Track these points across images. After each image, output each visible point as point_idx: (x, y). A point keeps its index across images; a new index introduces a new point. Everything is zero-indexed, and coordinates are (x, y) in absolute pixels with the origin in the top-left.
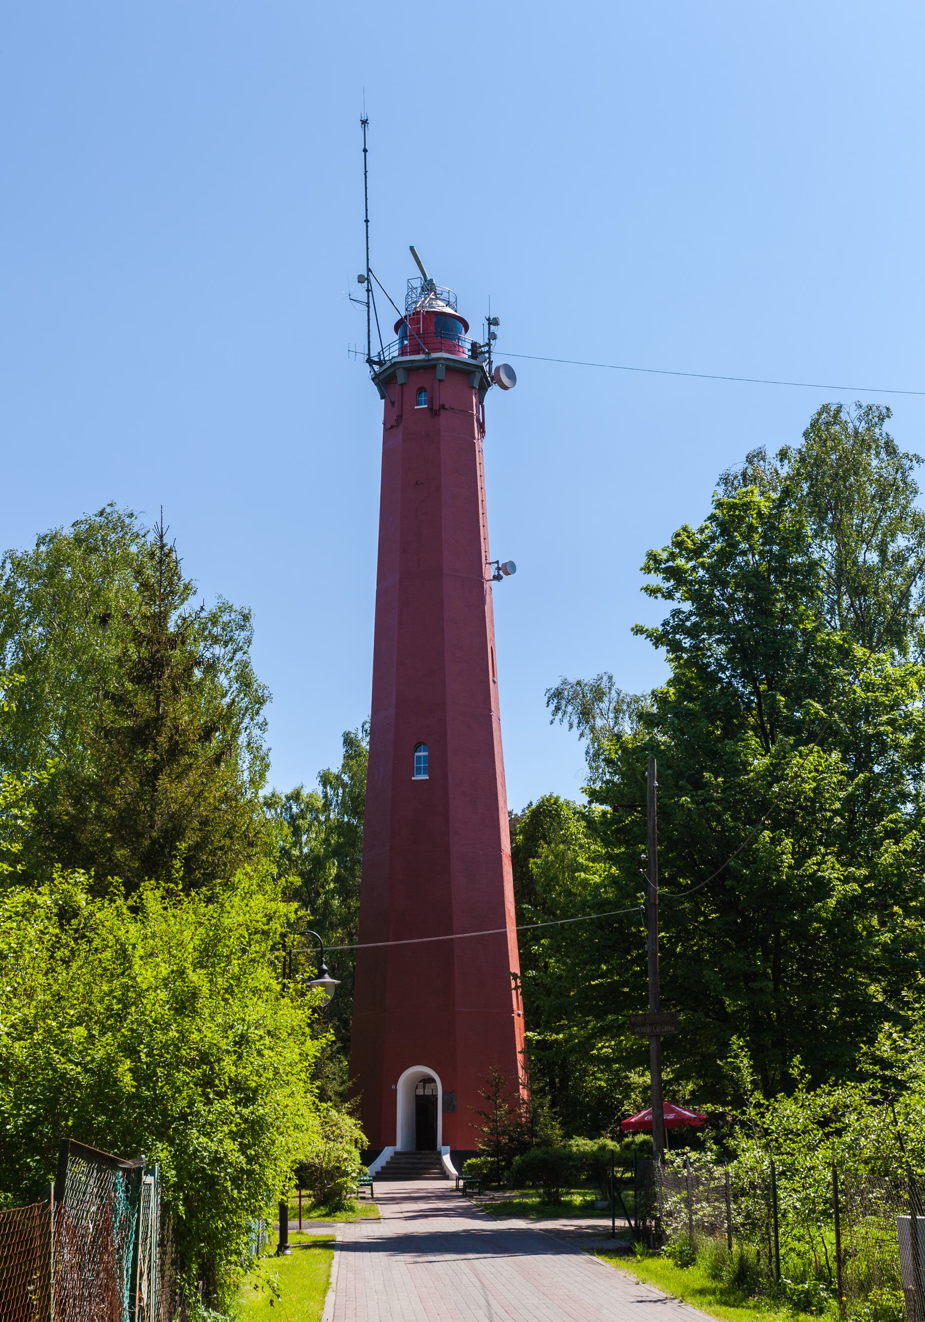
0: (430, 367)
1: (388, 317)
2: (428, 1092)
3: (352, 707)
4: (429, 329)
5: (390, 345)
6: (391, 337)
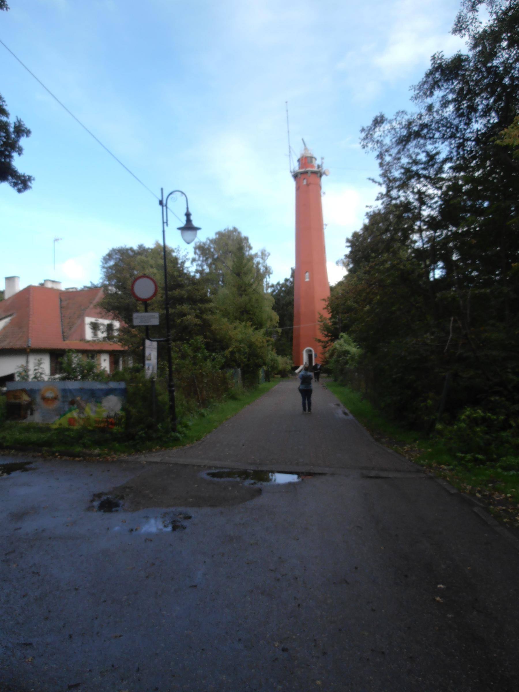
0: (306, 173)
5: (296, 166)
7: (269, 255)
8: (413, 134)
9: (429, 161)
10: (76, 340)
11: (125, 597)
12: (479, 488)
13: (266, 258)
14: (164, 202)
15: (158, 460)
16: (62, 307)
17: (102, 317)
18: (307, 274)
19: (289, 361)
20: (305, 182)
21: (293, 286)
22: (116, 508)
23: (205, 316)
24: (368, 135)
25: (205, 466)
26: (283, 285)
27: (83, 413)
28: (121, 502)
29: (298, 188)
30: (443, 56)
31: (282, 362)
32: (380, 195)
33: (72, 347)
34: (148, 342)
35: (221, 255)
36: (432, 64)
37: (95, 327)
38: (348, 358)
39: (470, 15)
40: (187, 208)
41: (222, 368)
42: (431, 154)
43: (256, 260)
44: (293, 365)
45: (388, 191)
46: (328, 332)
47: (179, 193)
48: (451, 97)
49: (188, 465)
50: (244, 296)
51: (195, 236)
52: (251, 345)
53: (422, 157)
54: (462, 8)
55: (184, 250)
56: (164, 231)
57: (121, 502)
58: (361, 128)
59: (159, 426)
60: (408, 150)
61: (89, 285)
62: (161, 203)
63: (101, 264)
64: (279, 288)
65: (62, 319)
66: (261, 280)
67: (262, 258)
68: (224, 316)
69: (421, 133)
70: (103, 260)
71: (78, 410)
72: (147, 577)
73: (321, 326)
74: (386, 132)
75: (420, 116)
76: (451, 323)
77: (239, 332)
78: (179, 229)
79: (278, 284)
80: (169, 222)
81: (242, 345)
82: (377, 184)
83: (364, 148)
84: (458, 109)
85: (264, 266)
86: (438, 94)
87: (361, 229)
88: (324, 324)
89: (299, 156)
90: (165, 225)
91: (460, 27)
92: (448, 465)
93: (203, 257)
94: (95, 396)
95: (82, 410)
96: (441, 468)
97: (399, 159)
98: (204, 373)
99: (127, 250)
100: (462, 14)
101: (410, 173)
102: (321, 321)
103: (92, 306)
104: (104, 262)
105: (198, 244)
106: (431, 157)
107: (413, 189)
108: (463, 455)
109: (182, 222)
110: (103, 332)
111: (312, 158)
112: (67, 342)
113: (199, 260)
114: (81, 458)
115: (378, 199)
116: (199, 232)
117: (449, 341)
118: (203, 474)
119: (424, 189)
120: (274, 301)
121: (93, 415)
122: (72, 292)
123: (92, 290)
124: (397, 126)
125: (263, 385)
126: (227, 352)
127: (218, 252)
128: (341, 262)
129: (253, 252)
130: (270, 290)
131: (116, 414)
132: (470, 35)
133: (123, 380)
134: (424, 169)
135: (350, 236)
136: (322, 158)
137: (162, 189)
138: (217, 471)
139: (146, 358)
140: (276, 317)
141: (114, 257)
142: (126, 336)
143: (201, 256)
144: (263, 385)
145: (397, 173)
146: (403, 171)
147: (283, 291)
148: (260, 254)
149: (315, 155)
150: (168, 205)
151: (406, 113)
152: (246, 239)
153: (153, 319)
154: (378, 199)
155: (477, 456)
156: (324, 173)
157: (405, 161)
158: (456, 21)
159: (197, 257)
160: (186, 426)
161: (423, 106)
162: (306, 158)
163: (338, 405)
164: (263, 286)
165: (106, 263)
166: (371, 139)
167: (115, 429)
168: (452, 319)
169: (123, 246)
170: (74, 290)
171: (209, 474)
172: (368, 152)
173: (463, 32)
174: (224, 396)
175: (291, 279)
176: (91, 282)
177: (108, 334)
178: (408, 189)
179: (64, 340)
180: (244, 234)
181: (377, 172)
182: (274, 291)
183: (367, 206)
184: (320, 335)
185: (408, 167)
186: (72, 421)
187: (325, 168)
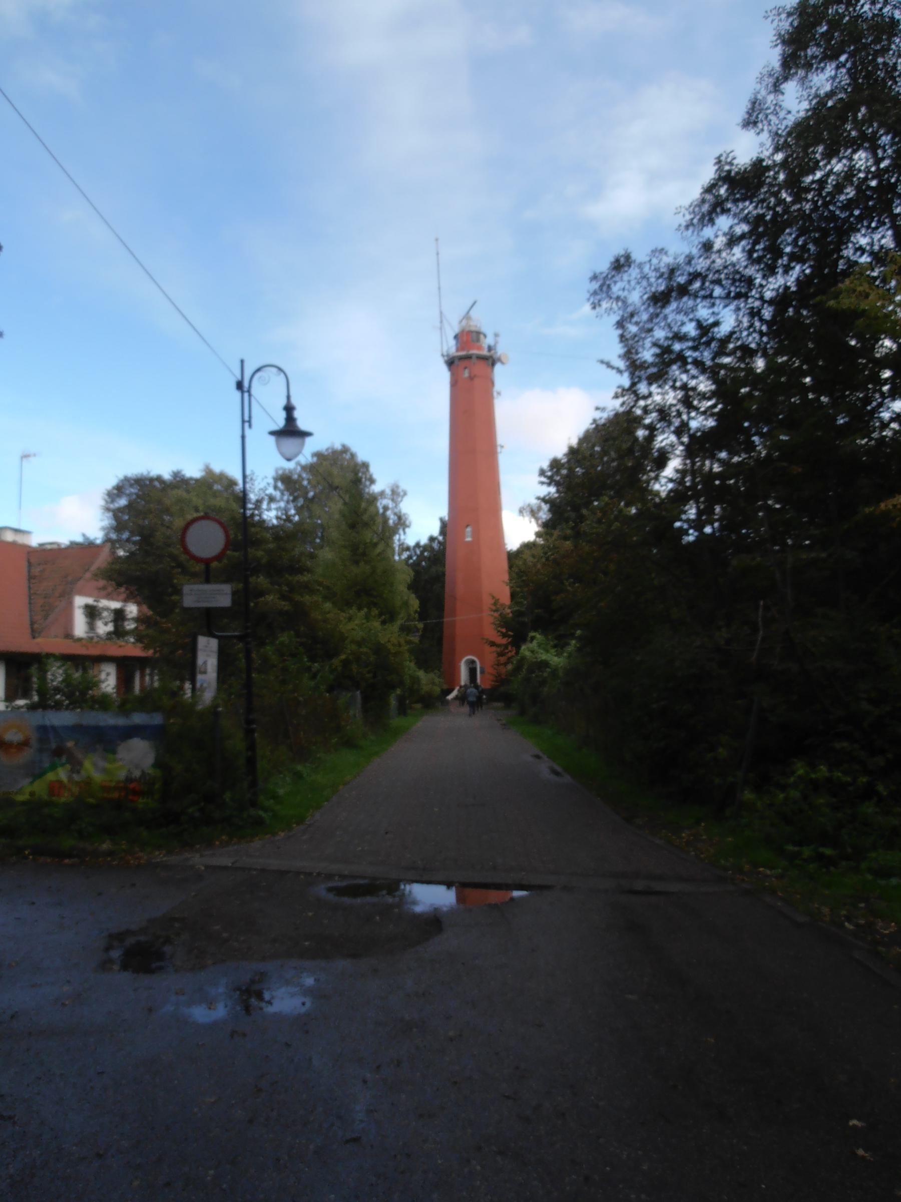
0: (468, 357)
1: (450, 335)
4: (468, 337)
5: (451, 346)
7: (405, 494)
8: (672, 290)
9: (702, 336)
10: (56, 637)
11: (211, 1172)
12: (844, 912)
13: (399, 499)
14: (246, 384)
15: (227, 861)
16: (31, 577)
17: (109, 597)
18: (469, 529)
19: (437, 680)
20: (466, 374)
21: (445, 549)
22: (158, 964)
23: (297, 598)
24: (603, 287)
25: (319, 874)
26: (425, 548)
27: (78, 772)
28: (167, 949)
29: (454, 384)
30: (734, 158)
31: (427, 680)
32: (620, 390)
33: (46, 649)
34: (202, 641)
35: (322, 492)
36: (717, 170)
37: (92, 613)
38: (545, 674)
39: (771, 97)
40: (288, 397)
41: (330, 689)
42: (705, 324)
43: (381, 503)
44: (445, 687)
45: (633, 384)
46: (508, 629)
47: (274, 370)
48: (744, 228)
49: (288, 872)
50: (362, 564)
51: (303, 444)
52: (379, 649)
53: (690, 329)
54: (758, 86)
55: (263, 479)
56: (243, 437)
57: (167, 949)
58: (591, 275)
59: (227, 796)
60: (666, 318)
61: (79, 539)
62: (240, 386)
63: (103, 503)
64: (418, 552)
65: (30, 599)
66: (391, 538)
67: (393, 500)
68: (326, 598)
69: (690, 288)
70: (106, 497)
71: (68, 767)
72: (251, 1121)
73: (495, 618)
74: (633, 283)
75: (689, 260)
76: (761, 610)
77: (355, 625)
78: (273, 433)
79: (418, 545)
80: (254, 421)
81: (364, 650)
82: (614, 371)
83: (594, 308)
84: (750, 253)
85: (395, 514)
86: (724, 222)
87: (565, 455)
88: (500, 615)
89: (457, 330)
90: (247, 425)
91: (753, 119)
92: (771, 868)
93: (290, 494)
94: (105, 740)
95: (76, 766)
96: (759, 873)
97: (650, 330)
98: (301, 699)
99: (152, 480)
100: (759, 97)
101: (667, 358)
102: (496, 611)
103: (88, 575)
104: (109, 500)
105: (280, 472)
106: (704, 329)
107: (675, 381)
108: (796, 849)
109: (280, 421)
110: (106, 624)
111: (478, 333)
112: (39, 640)
113: (282, 499)
114: (76, 860)
115: (616, 396)
116: (308, 440)
117: (759, 643)
118: (321, 890)
119: (693, 383)
120: (412, 574)
121: (98, 777)
122: (51, 550)
123: (86, 548)
124: (653, 275)
125: (396, 721)
126: (336, 662)
127: (314, 487)
128: (528, 509)
129: (376, 488)
130: (405, 555)
131: (143, 772)
132: (770, 131)
133: (156, 709)
134: (695, 348)
135: (545, 465)
136: (496, 335)
137: (242, 362)
138: (344, 884)
139: (198, 670)
140: (415, 603)
141: (128, 492)
142: (151, 631)
143: (286, 493)
144: (396, 721)
145: (648, 355)
146: (657, 351)
147: (425, 557)
148: (388, 492)
149: (484, 329)
150: (253, 392)
151: (666, 253)
152: (366, 466)
153: (220, 596)
154: (616, 396)
155: (821, 850)
156: (499, 360)
157: (660, 334)
158: (749, 106)
159: (277, 494)
160: (275, 797)
161: (696, 242)
162: (470, 333)
163: (537, 757)
164: (393, 549)
165: (113, 501)
166: (607, 293)
167: (141, 802)
168: (762, 603)
169: (145, 473)
170: (55, 546)
171: (330, 890)
172: (602, 316)
173: (760, 125)
174: (335, 740)
175: (441, 538)
176: (84, 535)
177: (116, 627)
178: (665, 382)
179: (34, 638)
180: (361, 457)
181: (614, 351)
182: (410, 557)
183: (597, 409)
184: (491, 633)
185: (666, 344)
186: (56, 788)
187: (500, 351)
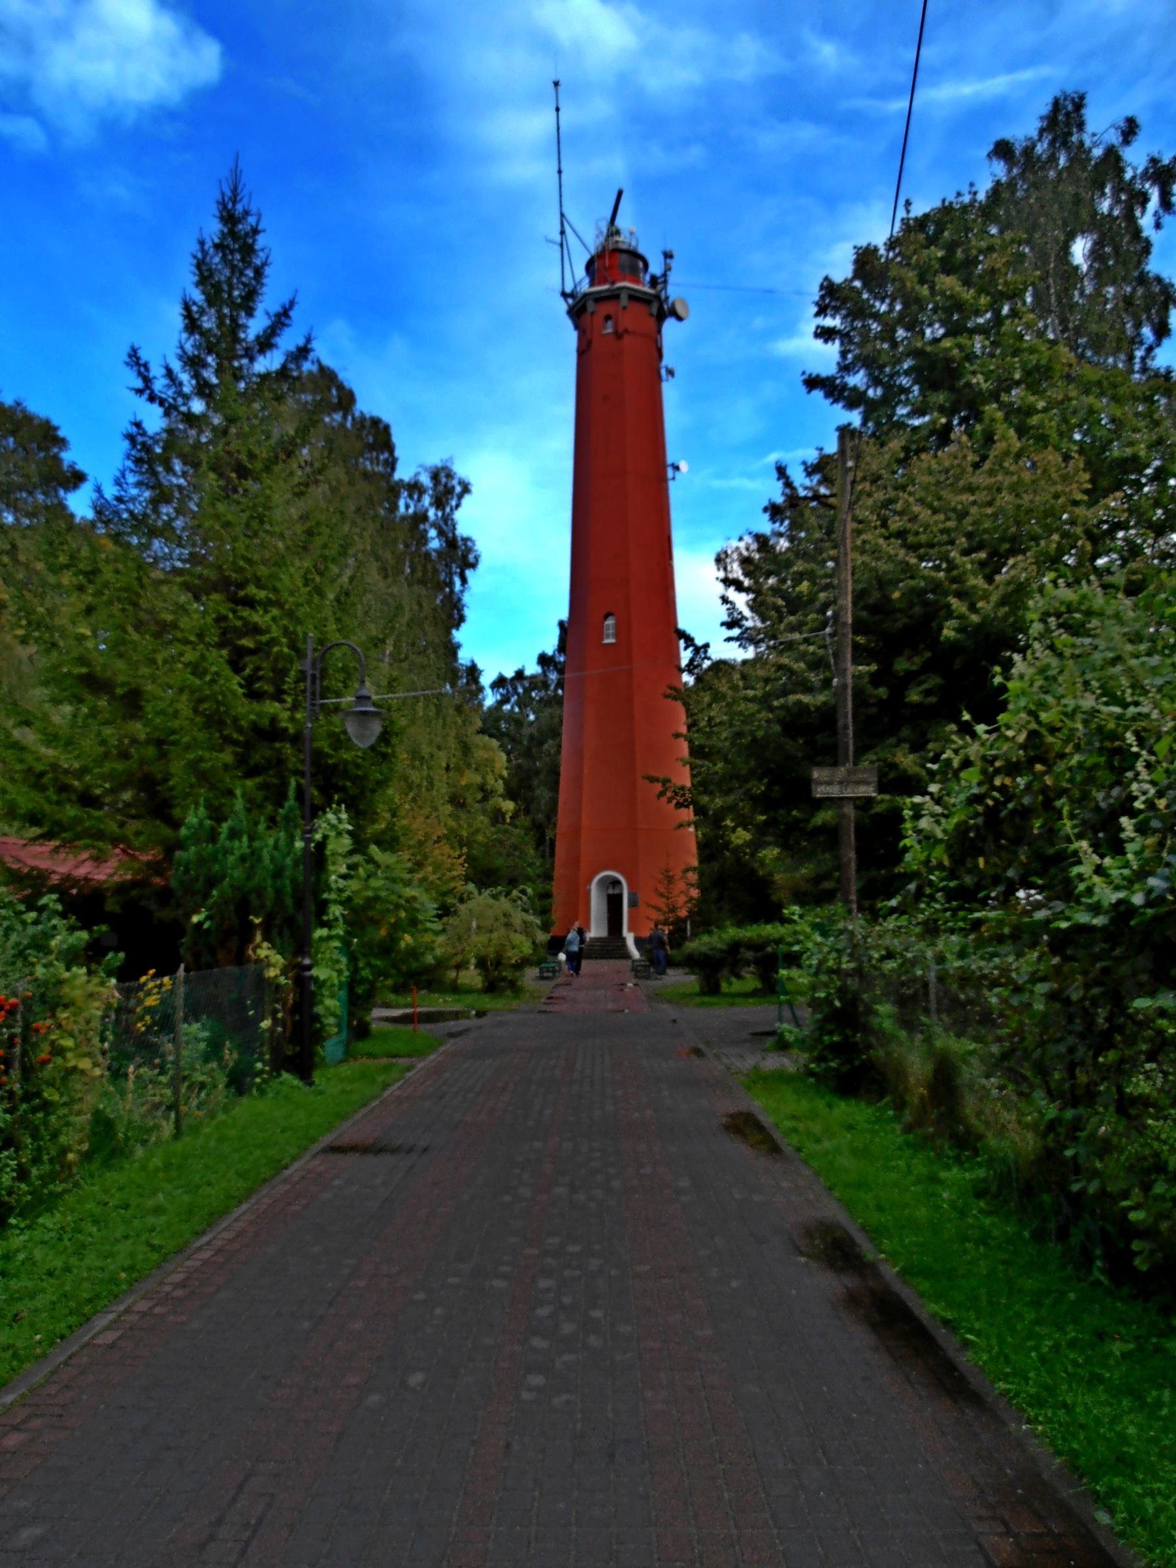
2: (617, 891)
3: (553, 601)
5: (578, 277)
6: (580, 272)
7: (466, 489)
18: (610, 622)
29: (583, 352)
136: (668, 255)
